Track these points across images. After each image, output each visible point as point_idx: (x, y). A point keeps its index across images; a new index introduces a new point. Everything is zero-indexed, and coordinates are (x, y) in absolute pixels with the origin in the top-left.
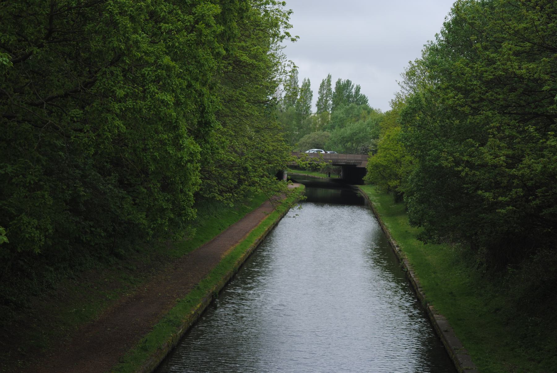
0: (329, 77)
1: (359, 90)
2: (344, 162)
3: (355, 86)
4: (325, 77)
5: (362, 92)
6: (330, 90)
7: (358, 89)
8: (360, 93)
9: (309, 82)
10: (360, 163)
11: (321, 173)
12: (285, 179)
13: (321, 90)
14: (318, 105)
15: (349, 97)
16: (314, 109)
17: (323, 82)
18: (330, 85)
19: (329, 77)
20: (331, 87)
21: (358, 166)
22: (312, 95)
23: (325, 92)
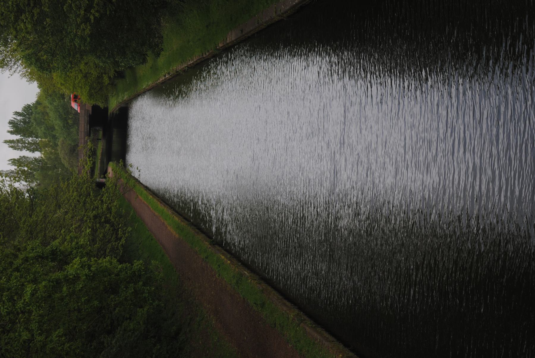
0: (6, 142)
1: (18, 113)
2: (87, 125)
3: (14, 116)
4: (6, 146)
5: (20, 110)
6: (18, 141)
7: (17, 113)
8: (20, 111)
9: (11, 160)
10: (88, 111)
11: (97, 147)
12: (104, 180)
13: (19, 148)
14: (33, 151)
15: (25, 122)
16: (37, 155)
17: (12, 147)
19: (6, 142)
20: (15, 139)
21: (91, 113)
22: (24, 156)
23: (20, 145)
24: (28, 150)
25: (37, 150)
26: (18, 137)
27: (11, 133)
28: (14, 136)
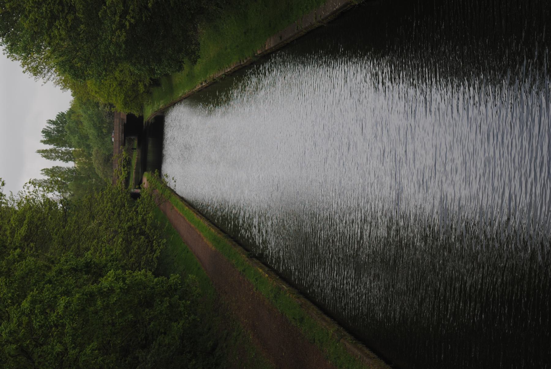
0: (39, 152)
3: (48, 125)
4: (39, 155)
6: (51, 151)
7: (51, 122)
8: (55, 120)
9: (44, 169)
11: (132, 156)
12: (139, 191)
13: (52, 158)
14: (67, 161)
16: (71, 165)
18: (46, 150)
19: (39, 152)
20: (48, 149)
21: (126, 122)
23: (53, 154)
24: (62, 159)
25: (71, 160)
26: (52, 147)
27: (45, 142)
28: (48, 145)
